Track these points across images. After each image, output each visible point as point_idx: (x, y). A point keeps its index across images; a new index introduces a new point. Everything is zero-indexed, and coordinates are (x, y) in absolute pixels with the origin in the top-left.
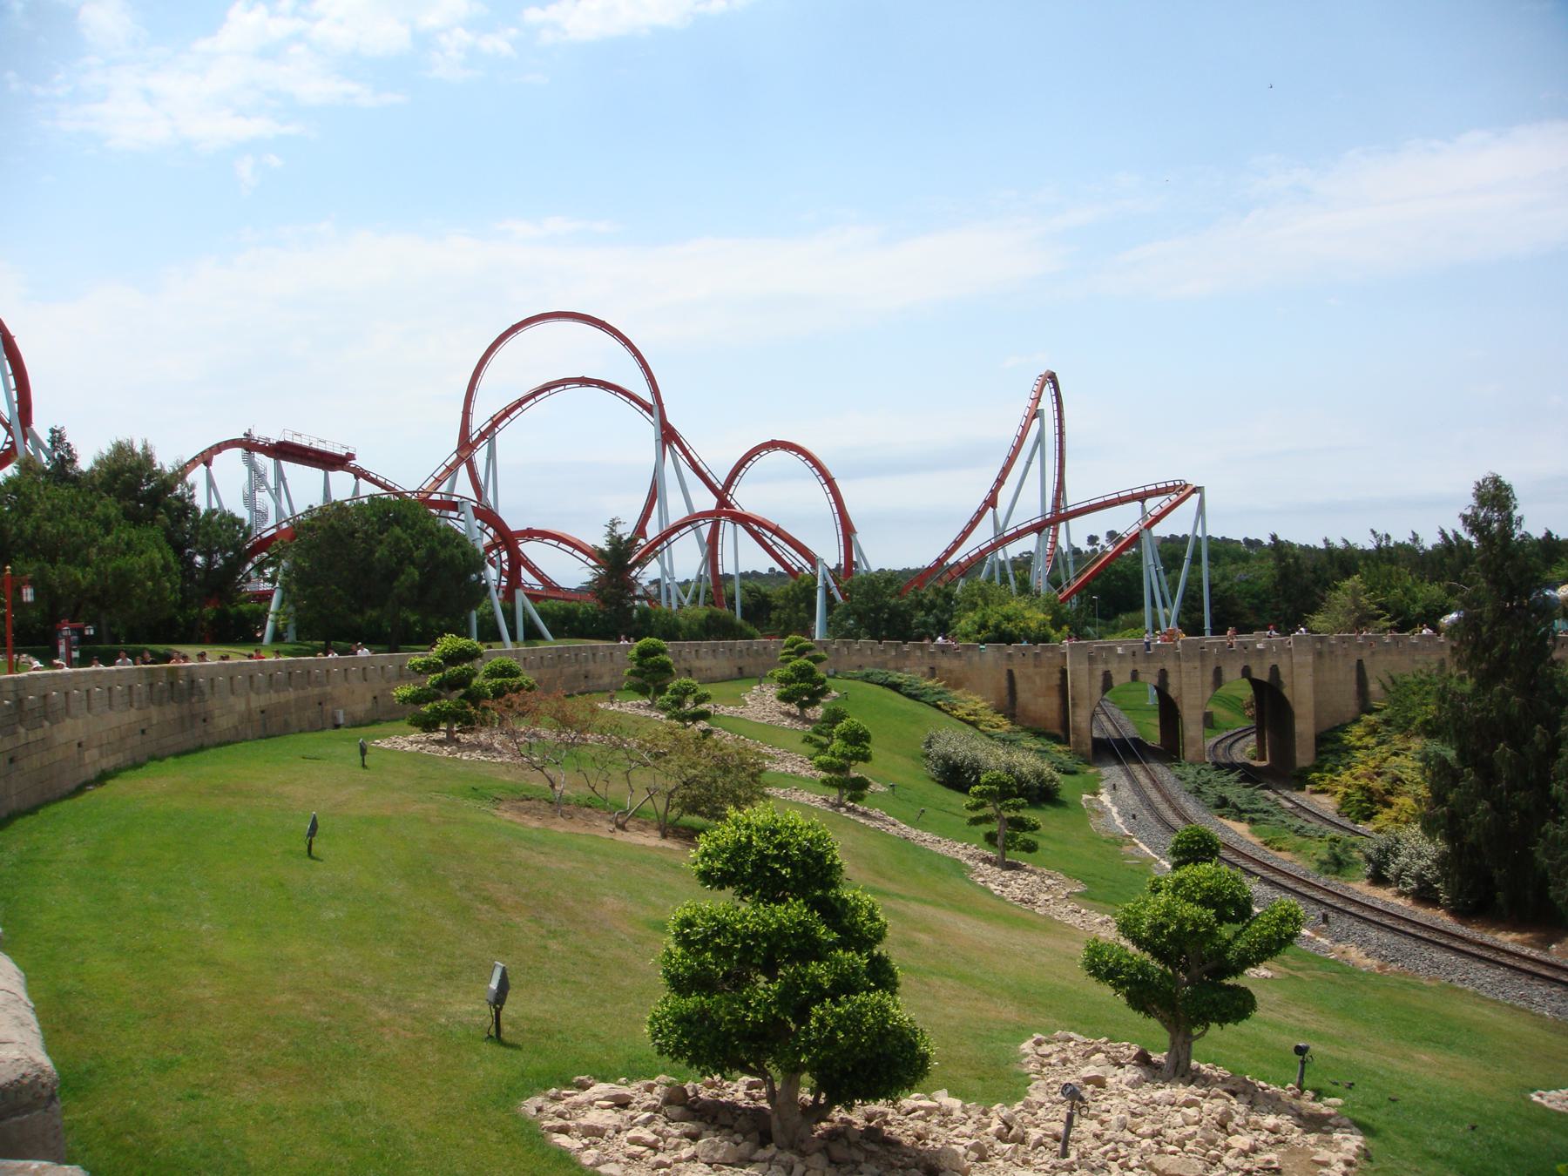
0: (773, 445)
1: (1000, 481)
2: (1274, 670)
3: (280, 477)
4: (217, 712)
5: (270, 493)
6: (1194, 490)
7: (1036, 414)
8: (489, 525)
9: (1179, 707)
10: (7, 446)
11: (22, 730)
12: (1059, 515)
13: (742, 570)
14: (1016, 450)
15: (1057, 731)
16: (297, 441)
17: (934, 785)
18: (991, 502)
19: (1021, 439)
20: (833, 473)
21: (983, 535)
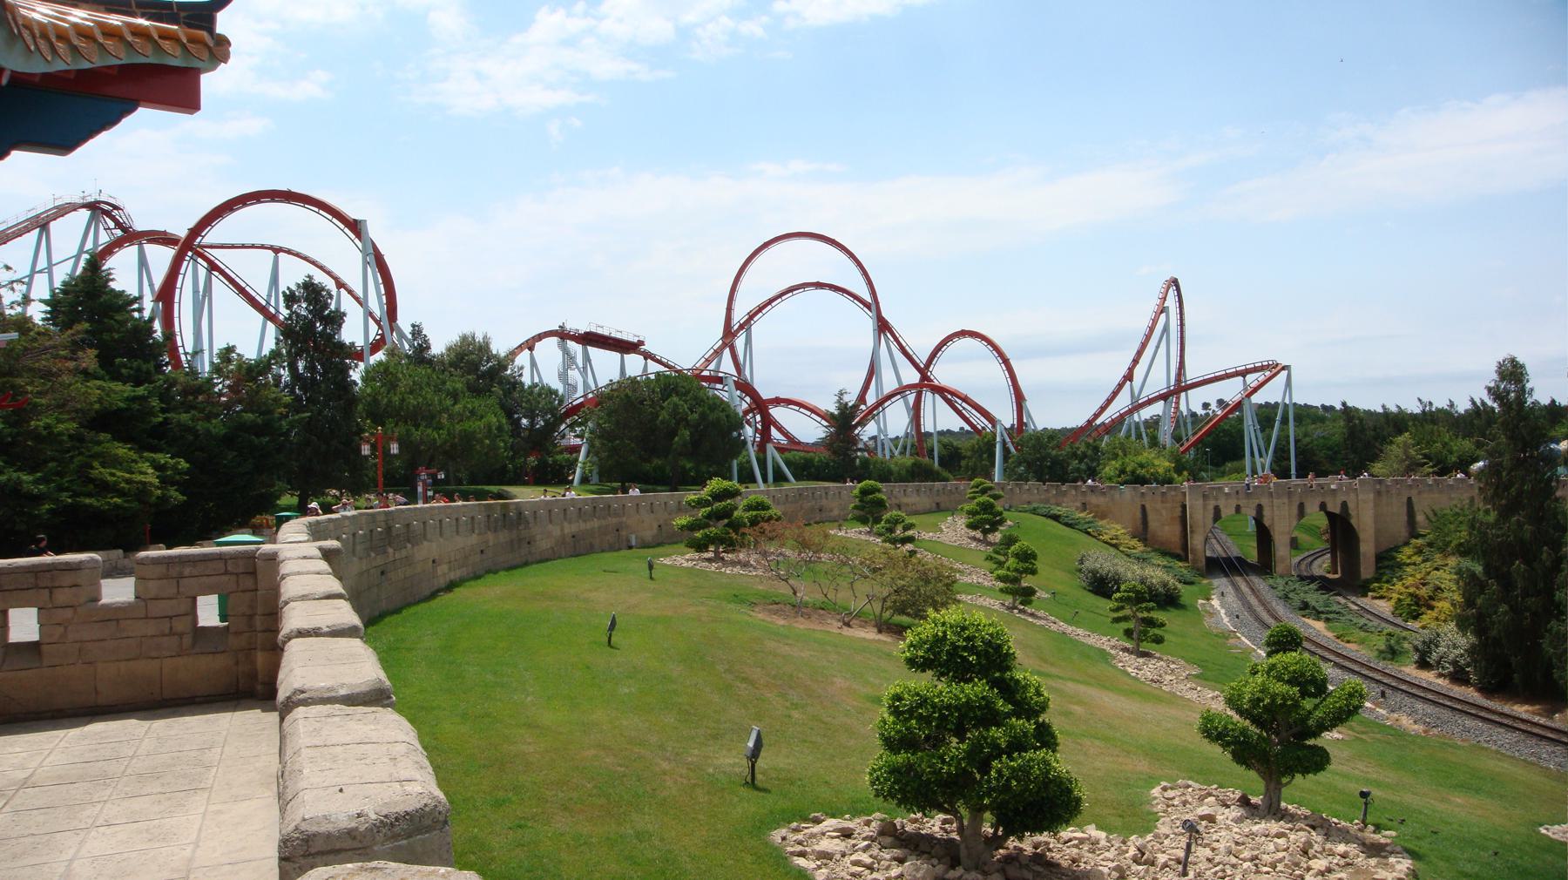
0: (963, 334)
1: (1136, 362)
2: (1344, 505)
3: (587, 358)
4: (538, 537)
5: (580, 371)
6: (1284, 368)
7: (1163, 310)
8: (747, 395)
9: (1272, 533)
10: (378, 337)
11: (390, 550)
12: (1181, 387)
13: (939, 429)
14: (1148, 337)
15: (1179, 551)
16: (600, 331)
17: (1086, 593)
18: (1129, 377)
19: (1152, 329)
20: (1008, 355)
21: (1122, 402)
